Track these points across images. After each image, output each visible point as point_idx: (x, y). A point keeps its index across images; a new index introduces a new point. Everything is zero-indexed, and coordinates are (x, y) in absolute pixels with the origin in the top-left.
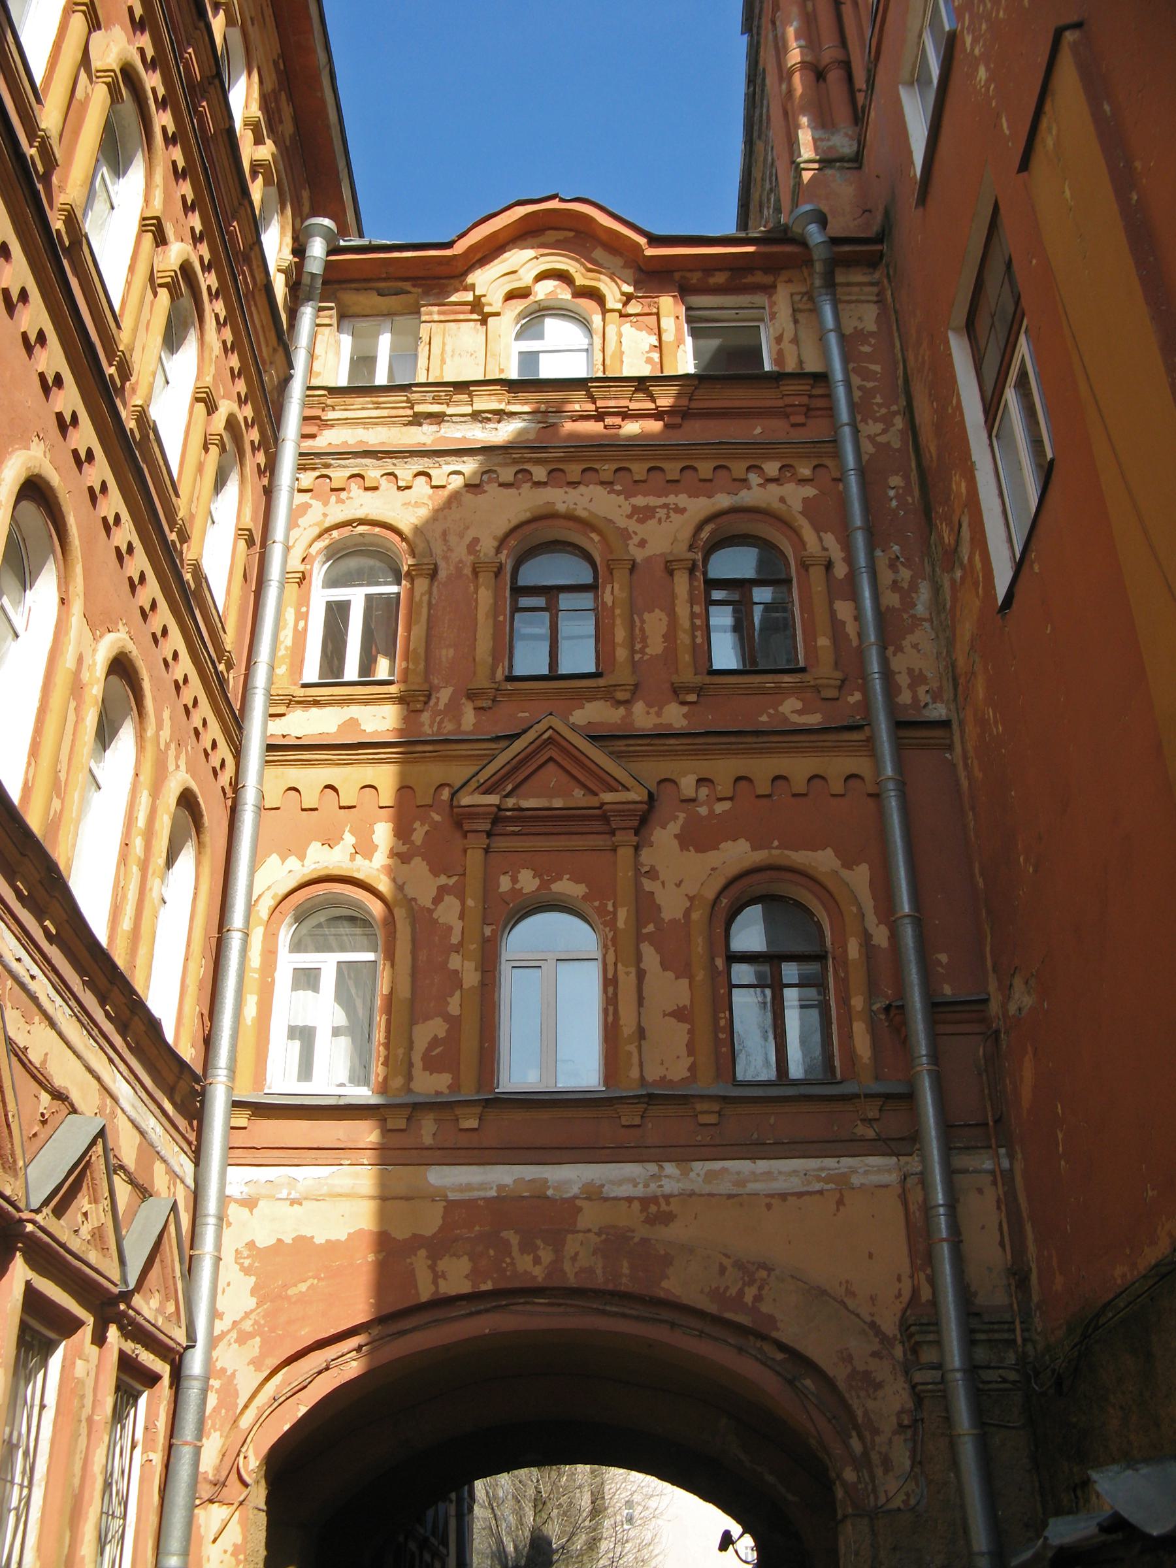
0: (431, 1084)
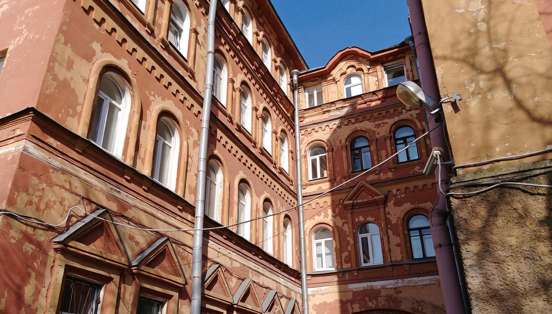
0: (346, 266)
